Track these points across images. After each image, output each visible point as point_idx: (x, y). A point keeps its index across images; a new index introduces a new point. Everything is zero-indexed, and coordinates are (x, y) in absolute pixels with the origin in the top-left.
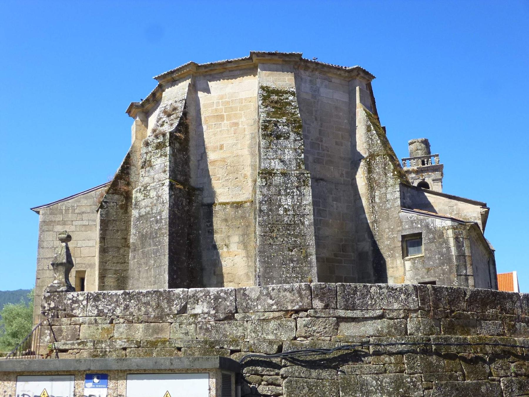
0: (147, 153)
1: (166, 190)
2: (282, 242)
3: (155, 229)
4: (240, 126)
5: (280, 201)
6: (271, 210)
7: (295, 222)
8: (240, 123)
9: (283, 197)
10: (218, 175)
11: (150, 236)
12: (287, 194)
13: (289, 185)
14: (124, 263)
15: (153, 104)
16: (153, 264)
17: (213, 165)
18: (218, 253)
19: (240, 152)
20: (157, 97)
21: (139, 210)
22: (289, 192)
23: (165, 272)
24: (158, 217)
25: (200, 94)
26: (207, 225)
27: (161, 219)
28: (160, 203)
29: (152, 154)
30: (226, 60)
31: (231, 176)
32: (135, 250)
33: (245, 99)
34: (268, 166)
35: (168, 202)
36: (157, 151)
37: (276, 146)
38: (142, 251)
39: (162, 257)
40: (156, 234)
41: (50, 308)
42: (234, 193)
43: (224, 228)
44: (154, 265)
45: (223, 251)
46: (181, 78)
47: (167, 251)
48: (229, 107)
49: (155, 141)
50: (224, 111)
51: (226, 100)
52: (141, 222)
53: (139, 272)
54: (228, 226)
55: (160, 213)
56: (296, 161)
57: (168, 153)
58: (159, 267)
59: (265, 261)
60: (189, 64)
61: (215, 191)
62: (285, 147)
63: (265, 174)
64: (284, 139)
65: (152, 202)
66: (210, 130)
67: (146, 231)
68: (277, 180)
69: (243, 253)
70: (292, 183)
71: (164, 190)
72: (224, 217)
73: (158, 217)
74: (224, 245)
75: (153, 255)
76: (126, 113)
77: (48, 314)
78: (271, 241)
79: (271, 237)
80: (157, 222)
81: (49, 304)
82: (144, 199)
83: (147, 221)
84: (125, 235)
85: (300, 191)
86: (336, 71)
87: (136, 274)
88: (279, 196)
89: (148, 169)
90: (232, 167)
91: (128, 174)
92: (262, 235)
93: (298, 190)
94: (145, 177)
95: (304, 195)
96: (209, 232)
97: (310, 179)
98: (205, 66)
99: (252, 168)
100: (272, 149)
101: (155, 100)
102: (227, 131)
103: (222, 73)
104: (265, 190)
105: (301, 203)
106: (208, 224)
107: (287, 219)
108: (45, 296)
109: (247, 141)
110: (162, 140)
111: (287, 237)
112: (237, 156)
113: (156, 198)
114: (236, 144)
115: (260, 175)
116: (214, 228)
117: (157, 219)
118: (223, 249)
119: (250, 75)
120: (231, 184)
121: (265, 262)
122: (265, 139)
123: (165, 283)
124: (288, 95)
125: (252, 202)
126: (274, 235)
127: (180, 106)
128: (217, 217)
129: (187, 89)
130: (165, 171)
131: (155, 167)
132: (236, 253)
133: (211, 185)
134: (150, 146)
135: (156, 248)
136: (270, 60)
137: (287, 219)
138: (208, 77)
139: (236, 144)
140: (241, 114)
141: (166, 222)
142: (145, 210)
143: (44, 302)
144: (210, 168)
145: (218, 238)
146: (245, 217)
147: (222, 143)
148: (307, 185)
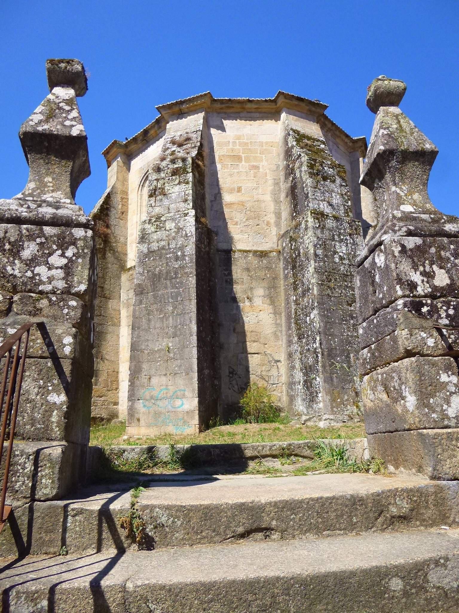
0: (157, 180)
1: (190, 221)
2: (341, 294)
3: (174, 268)
4: (261, 170)
5: (335, 246)
6: (326, 256)
7: (351, 273)
8: (261, 166)
9: (337, 243)
10: (235, 220)
11: (167, 276)
12: (341, 241)
13: (342, 231)
14: (100, 315)
15: (140, 145)
16: (171, 311)
17: (229, 208)
18: (238, 307)
19: (261, 197)
20: (149, 135)
21: (148, 245)
22: (343, 239)
23: (191, 322)
24: (179, 254)
25: (213, 131)
26: (225, 274)
27: (184, 255)
28: (182, 237)
29: (166, 180)
30: (248, 98)
31: (251, 222)
32: (142, 293)
33: (267, 143)
34: (317, 207)
35: (194, 236)
36: (174, 177)
37: (323, 187)
38: (153, 295)
39: (187, 303)
40: (176, 273)
41: (435, 288)
42: (255, 240)
43: (245, 277)
44: (173, 312)
45: (245, 305)
46: (191, 111)
47: (194, 295)
48: (247, 149)
49: (171, 166)
50: (241, 152)
51: (244, 141)
52: (152, 259)
53: (149, 320)
54: (251, 277)
55: (182, 248)
56: (344, 207)
57: (191, 179)
58: (180, 315)
59: (325, 315)
60: (205, 94)
61: (232, 236)
62: (333, 191)
63: (317, 214)
64: (331, 182)
65: (169, 235)
66: (226, 170)
67: (160, 270)
68: (330, 223)
69: (270, 309)
70: (345, 230)
71: (187, 221)
72: (245, 266)
73: (179, 254)
74: (246, 299)
75: (171, 300)
76: (103, 154)
77: (434, 310)
78: (329, 292)
79: (328, 287)
80: (177, 259)
81: (429, 276)
82: (156, 232)
83: (160, 258)
84: (102, 284)
85: (353, 240)
86: (344, 137)
87: (144, 323)
88: (333, 241)
89: (159, 198)
90: (253, 213)
91: (107, 215)
92: (319, 284)
93: (351, 238)
94: (156, 207)
95: (357, 244)
96: (226, 281)
97: (361, 228)
98: (222, 102)
99: (276, 216)
100: (320, 189)
101: (145, 140)
102: (245, 173)
103: (239, 113)
104: (319, 232)
105: (355, 253)
106: (226, 273)
107: (343, 269)
108: (403, 246)
109: (269, 187)
110: (180, 166)
111: (344, 289)
112: (258, 201)
113: (176, 230)
114: (256, 188)
115: (313, 215)
116: (234, 277)
117: (177, 255)
118: (244, 302)
119: (272, 120)
120: (251, 231)
121: (324, 315)
122: (311, 178)
123: (191, 335)
124: (319, 143)
125: (280, 252)
126: (332, 285)
127: (196, 138)
128: (236, 265)
129: (202, 120)
130: (186, 201)
131: (170, 195)
132: (261, 308)
133: (227, 229)
134: (162, 172)
135: (176, 290)
136: (296, 105)
137: (343, 269)
138: (223, 115)
139: (256, 188)
140: (262, 157)
141: (191, 260)
142: (157, 245)
143: (405, 266)
144: (226, 211)
145: (238, 289)
146: (271, 268)
147: (240, 185)
148: (359, 234)
